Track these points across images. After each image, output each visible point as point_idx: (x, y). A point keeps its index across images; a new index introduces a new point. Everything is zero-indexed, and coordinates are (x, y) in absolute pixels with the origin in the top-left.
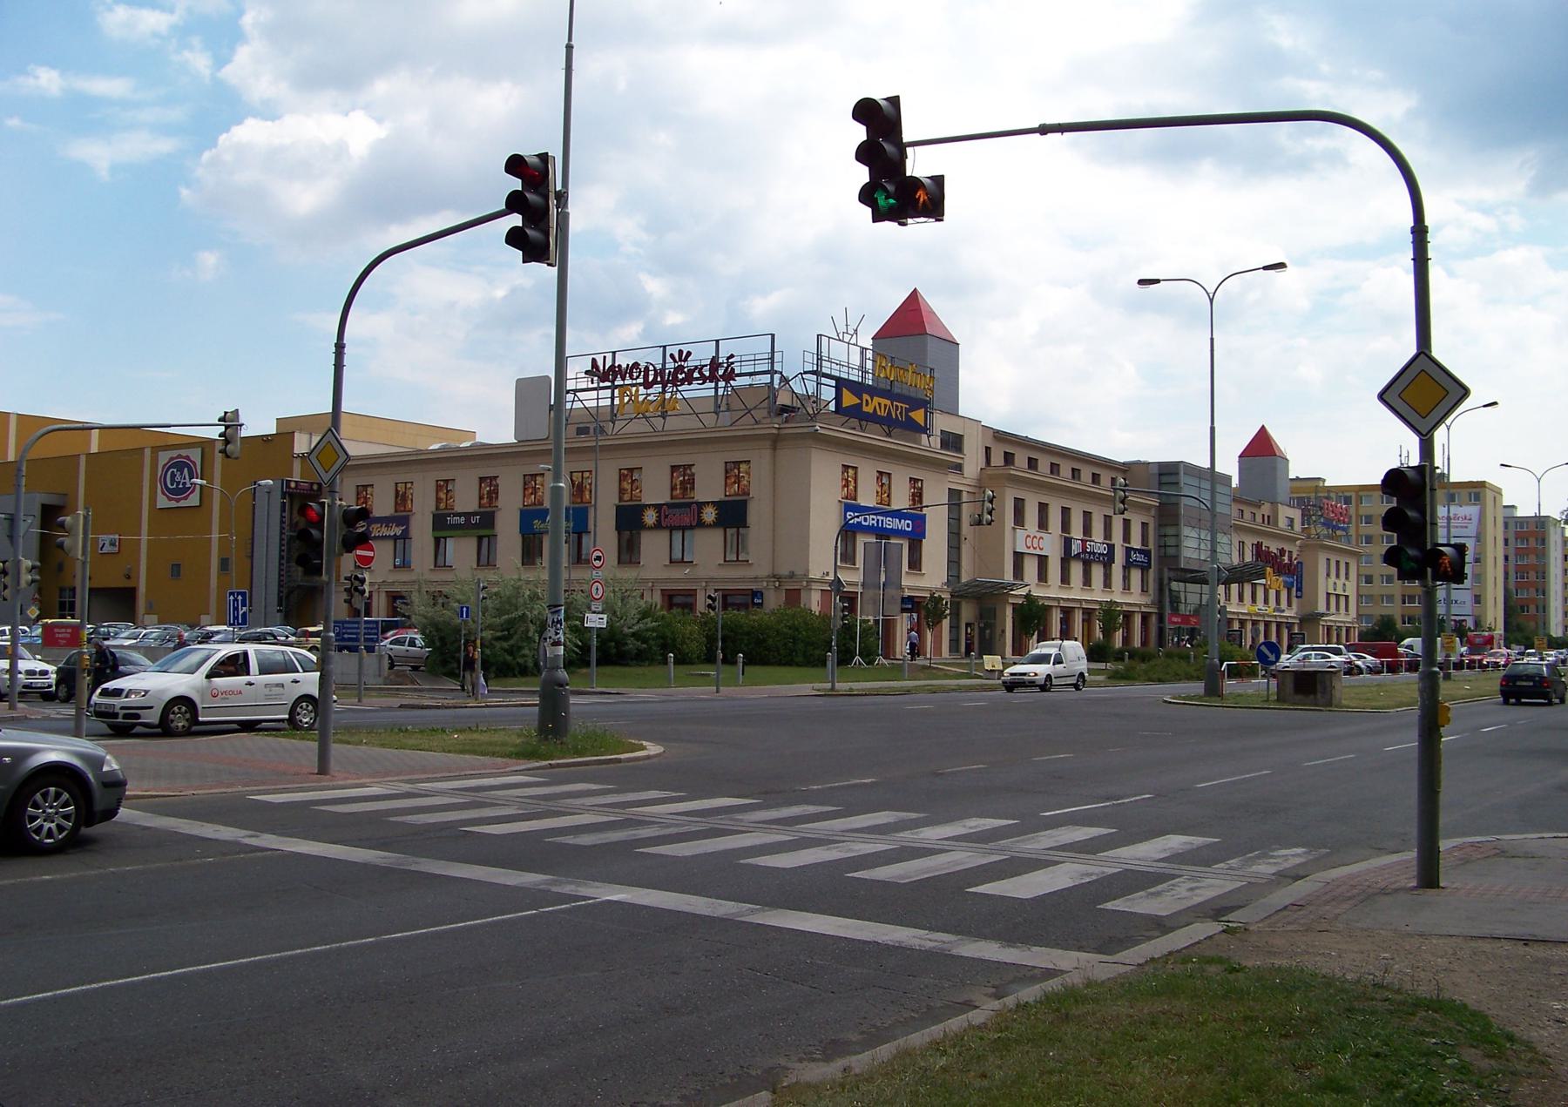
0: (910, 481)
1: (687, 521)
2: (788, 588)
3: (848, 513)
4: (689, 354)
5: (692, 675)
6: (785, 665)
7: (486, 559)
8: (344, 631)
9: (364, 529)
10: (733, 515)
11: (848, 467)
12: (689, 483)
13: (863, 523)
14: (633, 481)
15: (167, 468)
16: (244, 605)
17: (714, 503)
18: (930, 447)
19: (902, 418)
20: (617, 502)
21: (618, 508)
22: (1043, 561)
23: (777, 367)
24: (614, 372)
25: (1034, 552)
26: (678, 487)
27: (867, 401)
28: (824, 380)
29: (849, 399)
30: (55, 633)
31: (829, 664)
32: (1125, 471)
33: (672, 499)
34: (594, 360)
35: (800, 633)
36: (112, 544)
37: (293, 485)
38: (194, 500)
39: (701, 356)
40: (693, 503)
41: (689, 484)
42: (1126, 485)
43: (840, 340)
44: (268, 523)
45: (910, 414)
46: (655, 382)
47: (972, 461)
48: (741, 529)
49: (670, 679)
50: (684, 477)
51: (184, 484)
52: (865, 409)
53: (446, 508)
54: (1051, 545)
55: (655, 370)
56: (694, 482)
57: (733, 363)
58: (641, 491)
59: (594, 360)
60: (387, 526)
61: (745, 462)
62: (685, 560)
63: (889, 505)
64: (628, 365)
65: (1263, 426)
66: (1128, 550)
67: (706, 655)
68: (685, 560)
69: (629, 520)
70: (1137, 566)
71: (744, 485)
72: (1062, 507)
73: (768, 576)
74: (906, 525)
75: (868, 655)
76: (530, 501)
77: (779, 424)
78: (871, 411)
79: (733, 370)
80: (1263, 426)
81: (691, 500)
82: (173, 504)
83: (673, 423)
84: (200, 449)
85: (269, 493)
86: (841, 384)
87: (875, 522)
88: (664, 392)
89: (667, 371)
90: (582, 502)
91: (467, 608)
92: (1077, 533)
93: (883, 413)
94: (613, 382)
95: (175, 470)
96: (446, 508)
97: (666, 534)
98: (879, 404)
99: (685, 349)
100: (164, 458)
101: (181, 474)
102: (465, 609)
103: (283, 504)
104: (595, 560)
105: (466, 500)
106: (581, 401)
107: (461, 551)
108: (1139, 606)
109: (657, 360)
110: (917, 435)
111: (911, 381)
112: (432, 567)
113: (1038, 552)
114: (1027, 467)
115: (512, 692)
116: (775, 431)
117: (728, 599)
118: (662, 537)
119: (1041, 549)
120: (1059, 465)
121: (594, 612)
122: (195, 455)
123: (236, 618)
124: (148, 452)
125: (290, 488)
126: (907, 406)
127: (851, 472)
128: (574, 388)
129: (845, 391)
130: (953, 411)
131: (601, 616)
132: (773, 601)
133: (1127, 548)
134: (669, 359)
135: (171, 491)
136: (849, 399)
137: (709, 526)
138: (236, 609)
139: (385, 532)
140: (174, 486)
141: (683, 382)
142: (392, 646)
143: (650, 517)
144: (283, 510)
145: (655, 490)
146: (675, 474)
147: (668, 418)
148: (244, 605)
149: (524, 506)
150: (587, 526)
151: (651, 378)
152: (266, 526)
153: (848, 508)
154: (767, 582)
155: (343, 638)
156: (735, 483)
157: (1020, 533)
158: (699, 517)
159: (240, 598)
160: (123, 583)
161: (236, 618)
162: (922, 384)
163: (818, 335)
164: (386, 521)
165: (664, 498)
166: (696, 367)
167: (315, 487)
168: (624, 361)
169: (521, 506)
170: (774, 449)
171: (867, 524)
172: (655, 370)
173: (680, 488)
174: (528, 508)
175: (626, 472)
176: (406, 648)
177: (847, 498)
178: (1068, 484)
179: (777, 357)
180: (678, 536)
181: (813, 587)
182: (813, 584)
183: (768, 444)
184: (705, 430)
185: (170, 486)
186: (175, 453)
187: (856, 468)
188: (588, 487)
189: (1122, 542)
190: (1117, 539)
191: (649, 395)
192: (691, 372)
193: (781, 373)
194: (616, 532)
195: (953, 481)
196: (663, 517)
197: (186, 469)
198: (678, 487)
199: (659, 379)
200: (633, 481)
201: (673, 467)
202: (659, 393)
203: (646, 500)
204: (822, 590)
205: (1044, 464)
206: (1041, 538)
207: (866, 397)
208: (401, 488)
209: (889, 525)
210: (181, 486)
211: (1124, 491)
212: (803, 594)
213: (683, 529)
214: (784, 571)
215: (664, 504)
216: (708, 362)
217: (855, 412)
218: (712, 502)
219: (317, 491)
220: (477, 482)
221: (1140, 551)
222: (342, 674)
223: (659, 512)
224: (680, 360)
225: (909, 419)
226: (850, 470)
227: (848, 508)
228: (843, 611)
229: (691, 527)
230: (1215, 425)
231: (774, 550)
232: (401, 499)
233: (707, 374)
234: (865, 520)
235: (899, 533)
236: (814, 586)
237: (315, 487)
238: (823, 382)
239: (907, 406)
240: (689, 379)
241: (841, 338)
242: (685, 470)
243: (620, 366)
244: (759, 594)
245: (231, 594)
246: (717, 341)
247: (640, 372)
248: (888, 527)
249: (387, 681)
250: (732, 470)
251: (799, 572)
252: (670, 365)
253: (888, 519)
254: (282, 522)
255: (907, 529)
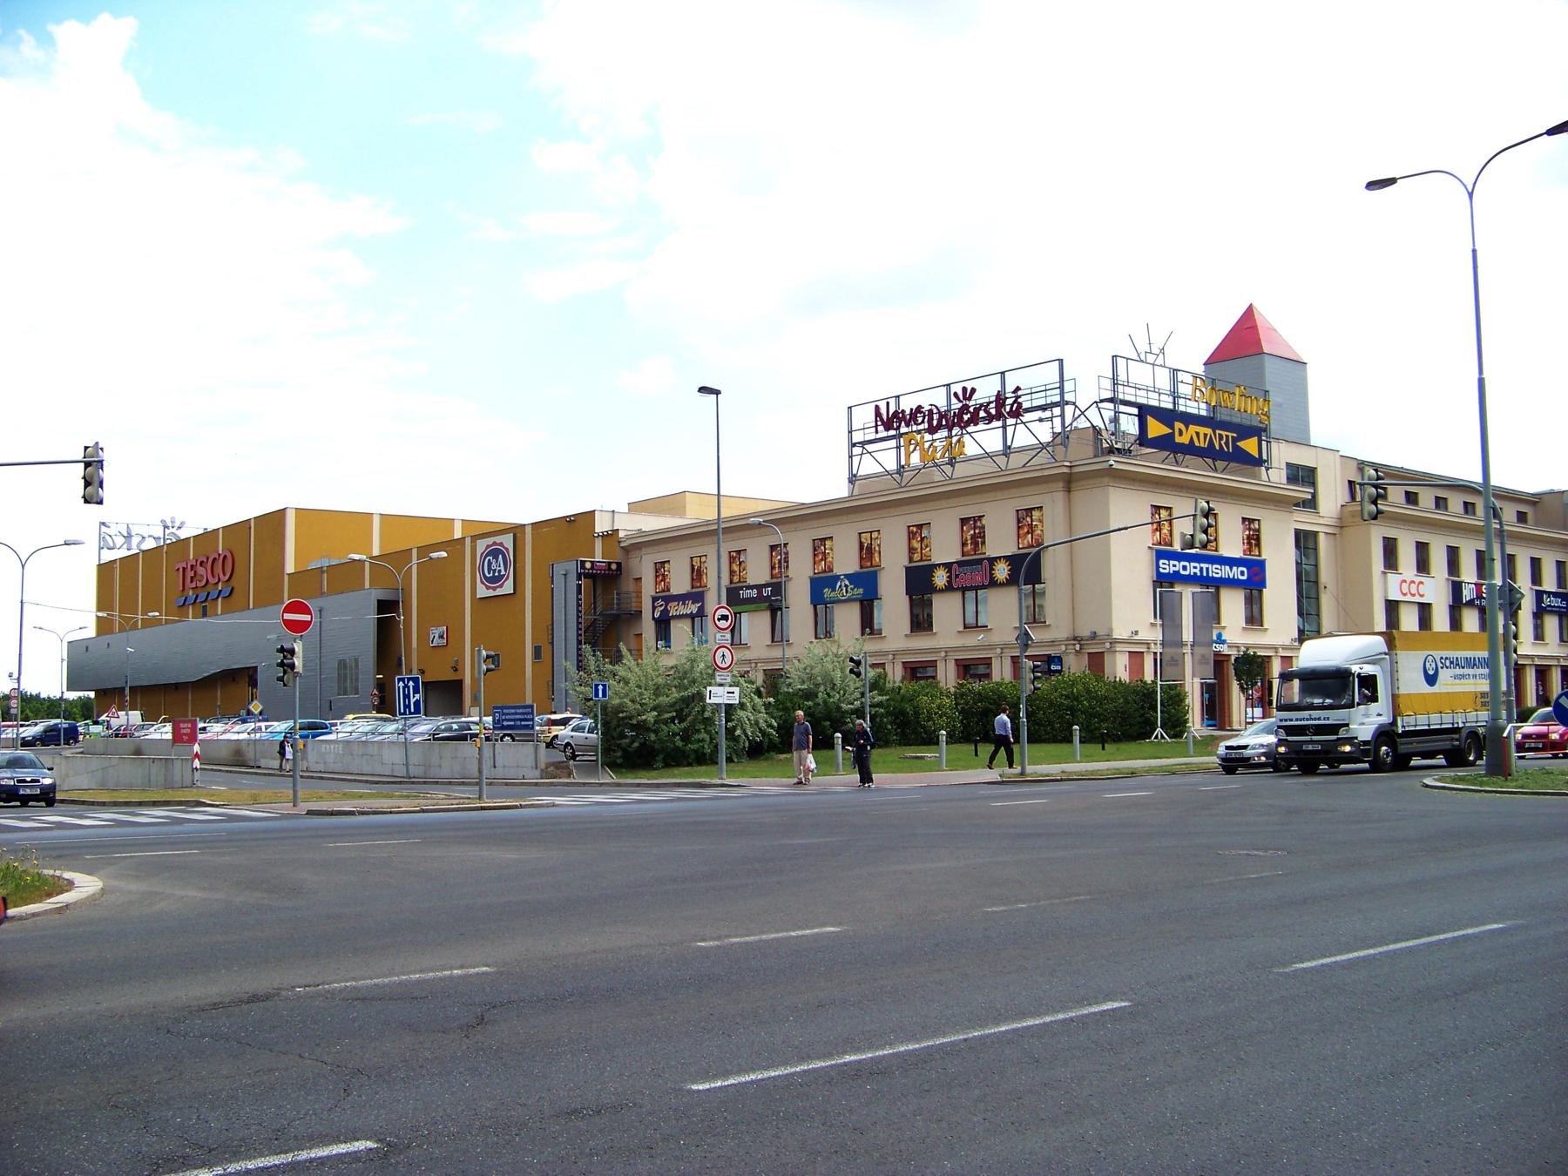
0: (1243, 522)
1: (978, 580)
2: (1090, 651)
3: (1161, 561)
4: (973, 390)
5: (906, 757)
6: (1061, 742)
7: (777, 634)
8: (504, 718)
9: (663, 607)
10: (1027, 569)
11: (1159, 508)
12: (980, 537)
13: (1182, 572)
14: (922, 539)
15: (484, 556)
16: (416, 691)
17: (1006, 558)
18: (1269, 481)
19: (1228, 448)
20: (906, 563)
21: (907, 569)
22: (1425, 610)
23: (1068, 397)
24: (898, 418)
25: (1413, 599)
26: (969, 542)
27: (1180, 430)
28: (1122, 408)
29: (1156, 429)
30: (180, 729)
31: (1077, 739)
32: (1534, 504)
33: (963, 556)
34: (877, 407)
35: (1080, 702)
36: (441, 637)
37: (588, 565)
38: (508, 588)
39: (986, 391)
40: (984, 559)
41: (979, 539)
42: (1379, 478)
43: (1142, 361)
44: (565, 607)
45: (1238, 444)
46: (939, 427)
47: (1332, 497)
48: (1036, 586)
49: (838, 765)
50: (973, 529)
51: (500, 571)
52: (1178, 439)
53: (740, 582)
54: (1435, 591)
55: (939, 412)
56: (984, 535)
57: (1020, 397)
58: (930, 550)
59: (877, 407)
60: (684, 604)
61: (1037, 508)
62: (979, 625)
63: (1216, 550)
64: (912, 409)
65: (1249, 313)
66: (1539, 595)
67: (962, 732)
68: (979, 625)
69: (919, 583)
70: (1552, 612)
71: (1038, 535)
72: (1417, 542)
73: (1068, 639)
74: (1238, 573)
75: (1174, 726)
76: (820, 568)
77: (1071, 462)
78: (1187, 442)
79: (1020, 405)
80: (1249, 313)
81: (982, 556)
82: (491, 593)
83: (961, 470)
84: (512, 534)
85: (565, 575)
86: (1144, 412)
87: (1197, 571)
88: (950, 437)
89: (952, 412)
90: (872, 566)
91: (604, 686)
92: (1468, 574)
93: (1203, 444)
94: (898, 428)
95: (491, 558)
96: (740, 582)
97: (957, 596)
98: (1198, 434)
99: (969, 385)
100: (482, 545)
101: (497, 562)
102: (600, 687)
103: (579, 586)
104: (719, 620)
105: (757, 572)
106: (870, 453)
107: (755, 626)
108: (1557, 658)
109: (941, 403)
110: (1257, 468)
111: (1241, 407)
112: (769, 643)
113: (1418, 599)
114: (1516, 521)
115: (639, 785)
116: (1065, 470)
117: (966, 668)
118: (954, 599)
119: (1422, 596)
120: (1446, 499)
121: (721, 685)
122: (507, 541)
123: (407, 706)
124: (468, 541)
125: (585, 568)
126: (1235, 435)
127: (1164, 513)
128: (862, 440)
129: (1151, 421)
130: (1304, 442)
131: (731, 689)
132: (1075, 666)
133: (1536, 591)
134: (954, 400)
135: (487, 579)
136: (1156, 429)
137: (1002, 585)
138: (407, 696)
139: (683, 610)
140: (491, 575)
141: (968, 423)
142: (573, 733)
143: (940, 578)
144: (579, 592)
145: (945, 548)
146: (965, 528)
147: (957, 465)
148: (416, 691)
149: (815, 573)
150: (877, 592)
151: (935, 423)
152: (563, 610)
153: (1160, 555)
154: (1066, 645)
155: (503, 725)
156: (1028, 533)
157: (1393, 579)
158: (991, 574)
159: (411, 684)
160: (450, 676)
161: (407, 706)
162: (1252, 407)
163: (1113, 357)
164: (682, 598)
165: (954, 555)
166: (981, 405)
167: (614, 567)
168: (907, 405)
169: (812, 574)
170: (1069, 490)
171: (1187, 573)
172: (939, 412)
173: (971, 543)
174: (821, 575)
175: (915, 529)
176: (586, 735)
177: (1160, 544)
178: (1514, 529)
179: (1068, 386)
180: (970, 595)
181: (1118, 649)
182: (1117, 645)
183: (1060, 485)
184: (1001, 474)
185: (488, 575)
186: (490, 541)
187: (1170, 508)
188: (877, 548)
189: (1530, 585)
190: (1523, 582)
191: (934, 440)
192: (977, 410)
193: (1074, 404)
194: (907, 597)
195: (1305, 521)
196: (953, 577)
197: (500, 556)
198: (969, 542)
199: (944, 423)
200: (922, 539)
201: (962, 520)
202: (946, 438)
203: (936, 560)
204: (1129, 652)
205: (1427, 498)
206: (1421, 583)
207: (1178, 425)
208: (696, 563)
209: (1217, 573)
210: (497, 574)
211: (1376, 487)
212: (1107, 658)
213: (976, 589)
214: (1086, 633)
215: (954, 563)
216: (993, 399)
217: (1165, 443)
218: (1004, 557)
219: (616, 570)
220: (767, 550)
221: (1555, 595)
222: (504, 767)
223: (949, 571)
224: (965, 398)
225: (1236, 447)
226: (1163, 512)
227: (1160, 555)
228: (1033, 672)
229: (983, 587)
230: (1485, 375)
231: (1073, 608)
232: (697, 574)
233: (993, 411)
234: (1185, 568)
235: (1232, 583)
236: (1119, 647)
237: (614, 567)
238: (1120, 410)
239: (1235, 435)
240: (975, 420)
241: (1143, 358)
242: (975, 522)
243: (903, 411)
244: (1056, 660)
245: (399, 680)
246: (1003, 373)
247: (924, 417)
248: (1215, 575)
249: (545, 774)
250: (1024, 519)
251: (1101, 632)
252: (956, 405)
253: (1215, 566)
254: (579, 605)
255: (1241, 578)
